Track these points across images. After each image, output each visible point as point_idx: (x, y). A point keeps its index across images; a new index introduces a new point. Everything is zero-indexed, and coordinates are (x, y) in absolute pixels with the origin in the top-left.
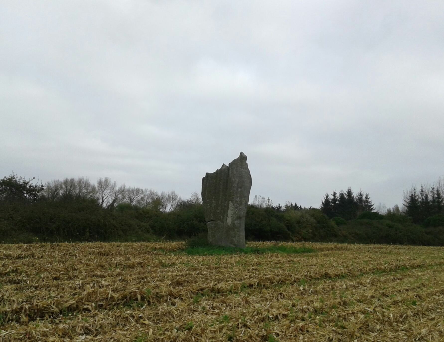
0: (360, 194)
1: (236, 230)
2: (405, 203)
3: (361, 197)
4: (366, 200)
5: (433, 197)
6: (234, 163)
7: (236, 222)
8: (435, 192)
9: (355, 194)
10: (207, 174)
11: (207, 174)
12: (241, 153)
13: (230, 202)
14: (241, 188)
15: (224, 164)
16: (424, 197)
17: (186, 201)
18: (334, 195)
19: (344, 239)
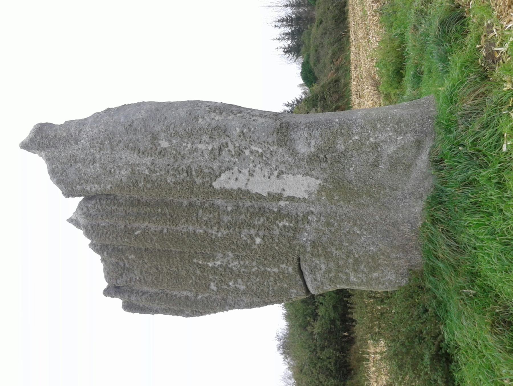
1: (340, 146)
2: (293, 60)
4: (291, 106)
6: (66, 180)
8: (280, 24)
11: (107, 292)
12: (26, 146)
13: (216, 185)
14: (155, 137)
15: (71, 220)
16: (287, 37)
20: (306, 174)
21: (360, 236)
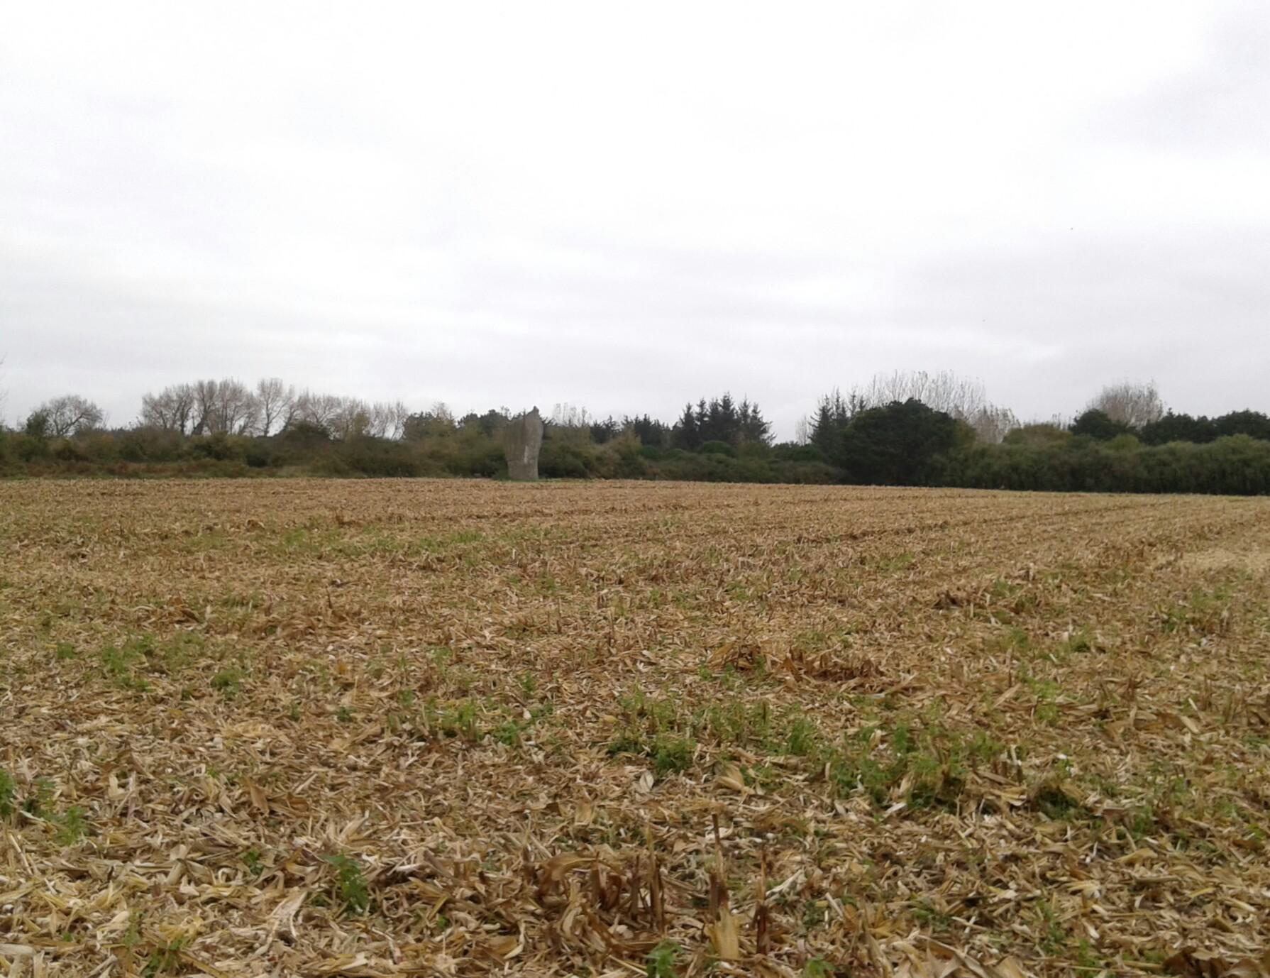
9: (736, 406)
18: (702, 405)
19: (653, 477)
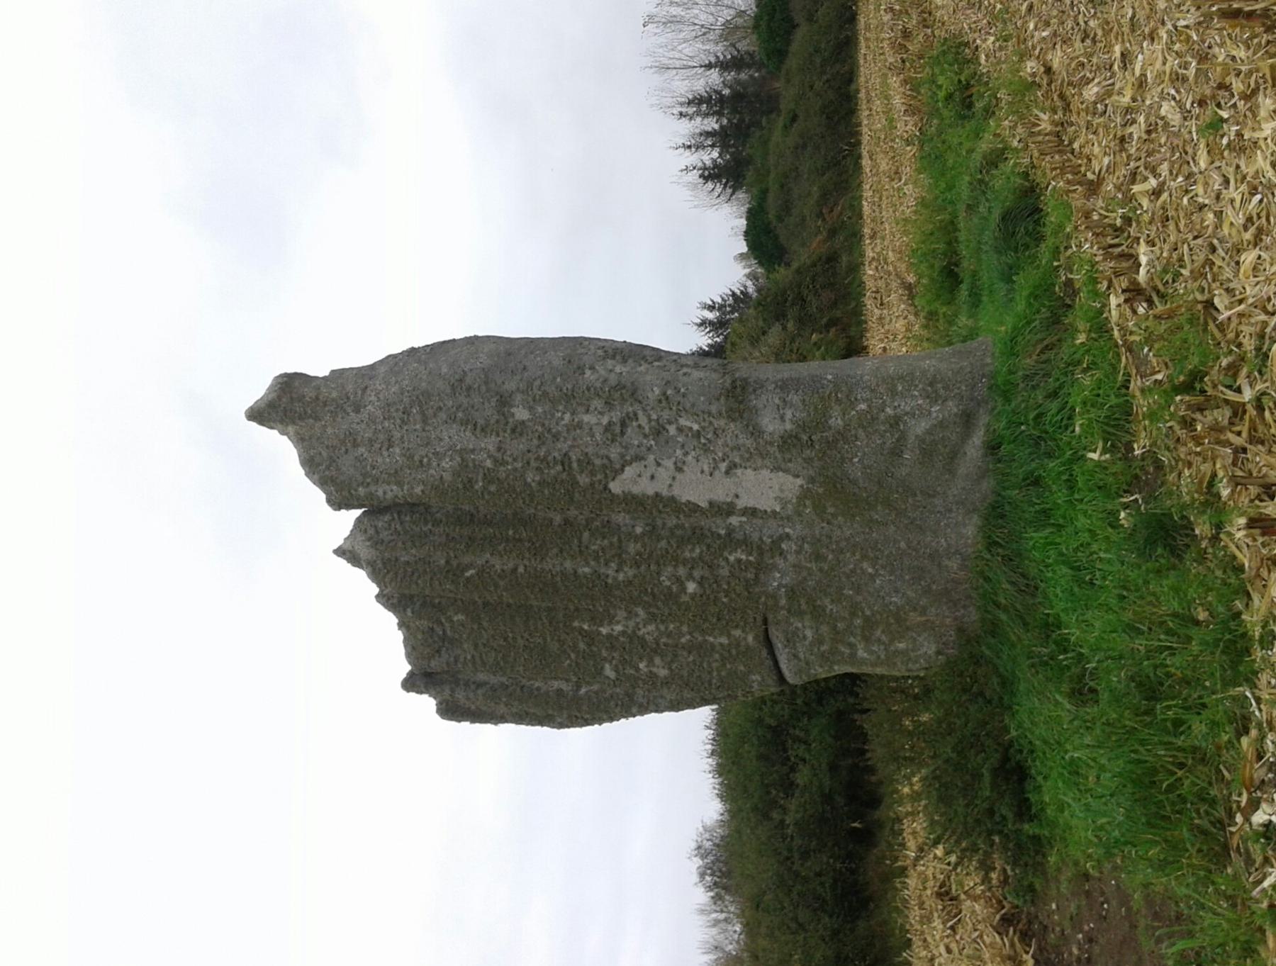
0: (700, 325)
1: (836, 421)
3: (711, 323)
5: (706, 115)
6: (320, 466)
7: (771, 425)
10: (410, 684)
11: (410, 684)
12: (259, 414)
13: (615, 487)
14: (504, 402)
15: (340, 552)
17: (698, 862)
20: (777, 469)
21: (872, 577)
